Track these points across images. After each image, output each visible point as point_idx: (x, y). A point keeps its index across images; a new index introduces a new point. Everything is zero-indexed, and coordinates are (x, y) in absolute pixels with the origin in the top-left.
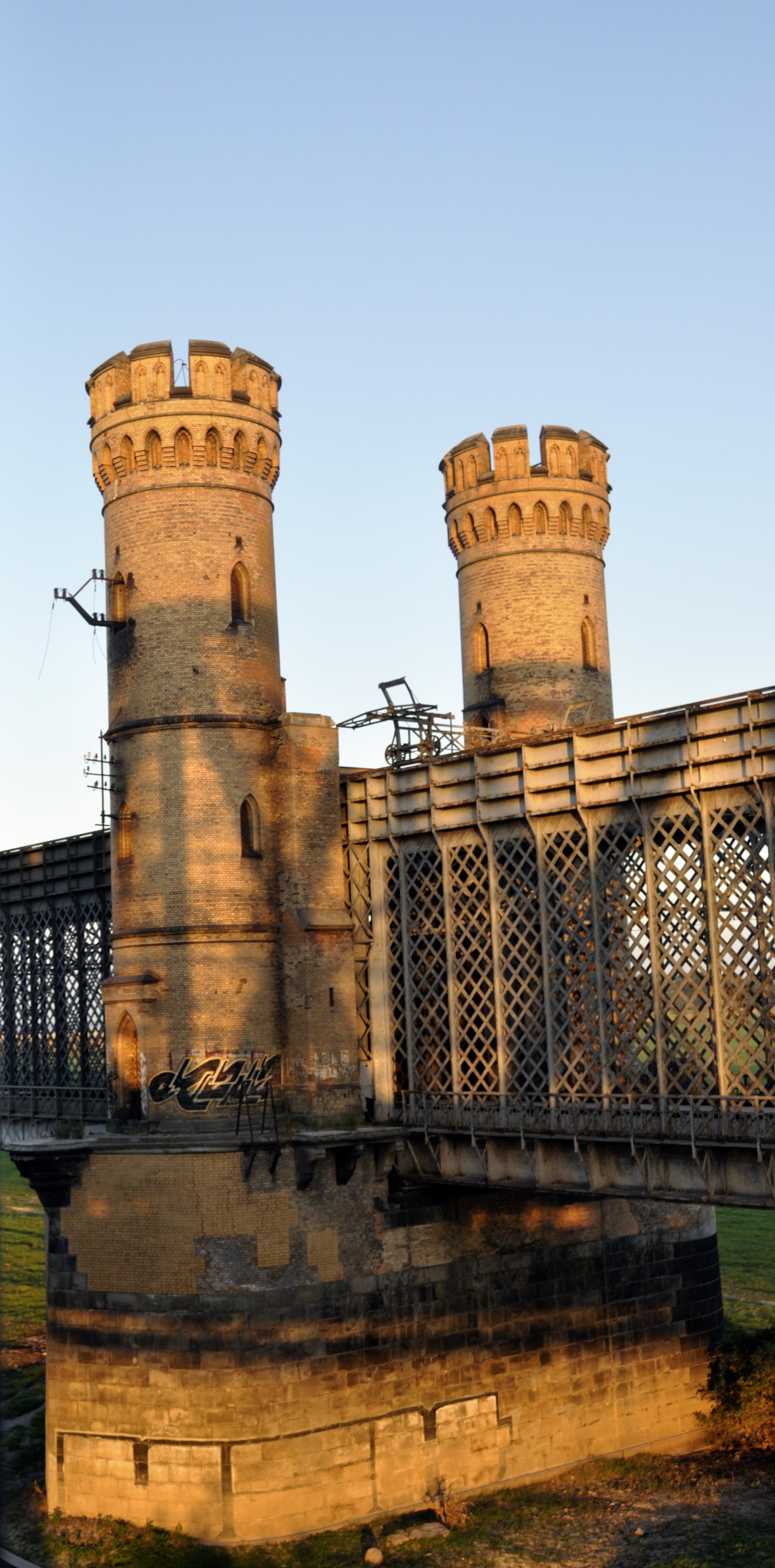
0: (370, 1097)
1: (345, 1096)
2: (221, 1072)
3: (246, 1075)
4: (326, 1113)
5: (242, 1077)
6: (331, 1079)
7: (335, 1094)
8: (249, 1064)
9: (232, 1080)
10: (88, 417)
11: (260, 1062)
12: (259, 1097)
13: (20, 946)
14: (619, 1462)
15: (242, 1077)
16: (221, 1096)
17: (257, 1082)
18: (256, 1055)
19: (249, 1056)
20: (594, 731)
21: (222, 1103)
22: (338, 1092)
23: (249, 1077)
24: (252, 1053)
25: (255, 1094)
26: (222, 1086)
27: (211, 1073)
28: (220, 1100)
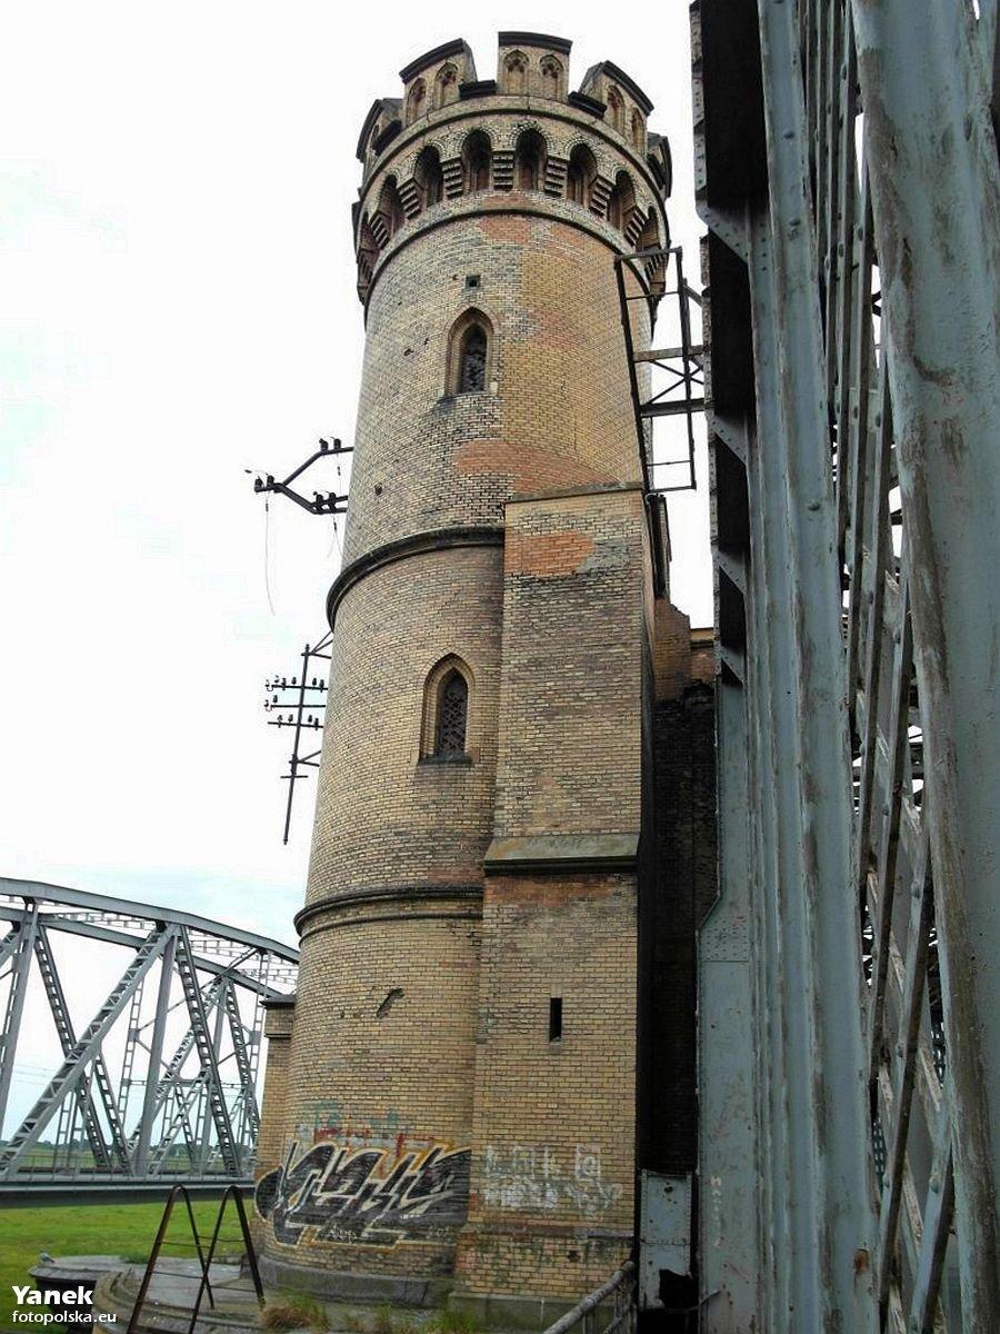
0: (680, 1267)
1: (573, 1256)
2: (333, 1173)
3: (382, 1183)
4: (501, 1295)
5: (371, 1187)
6: (537, 1211)
7: (538, 1250)
8: (390, 1163)
9: (351, 1192)
10: (734, 1305)
11: (419, 1158)
12: (402, 1233)
13: (491, 1138)
14: (382, 190)
15: (371, 1187)
16: (321, 1222)
17: (405, 1201)
18: (410, 1143)
19: (392, 1144)
20: (762, 1225)
21: (320, 1237)
22: (550, 1246)
23: (386, 1189)
24: (401, 1140)
25: (393, 1224)
26: (332, 1201)
27: (318, 1172)
28: (319, 1229)
